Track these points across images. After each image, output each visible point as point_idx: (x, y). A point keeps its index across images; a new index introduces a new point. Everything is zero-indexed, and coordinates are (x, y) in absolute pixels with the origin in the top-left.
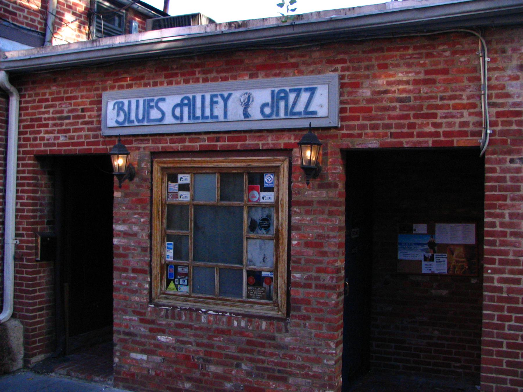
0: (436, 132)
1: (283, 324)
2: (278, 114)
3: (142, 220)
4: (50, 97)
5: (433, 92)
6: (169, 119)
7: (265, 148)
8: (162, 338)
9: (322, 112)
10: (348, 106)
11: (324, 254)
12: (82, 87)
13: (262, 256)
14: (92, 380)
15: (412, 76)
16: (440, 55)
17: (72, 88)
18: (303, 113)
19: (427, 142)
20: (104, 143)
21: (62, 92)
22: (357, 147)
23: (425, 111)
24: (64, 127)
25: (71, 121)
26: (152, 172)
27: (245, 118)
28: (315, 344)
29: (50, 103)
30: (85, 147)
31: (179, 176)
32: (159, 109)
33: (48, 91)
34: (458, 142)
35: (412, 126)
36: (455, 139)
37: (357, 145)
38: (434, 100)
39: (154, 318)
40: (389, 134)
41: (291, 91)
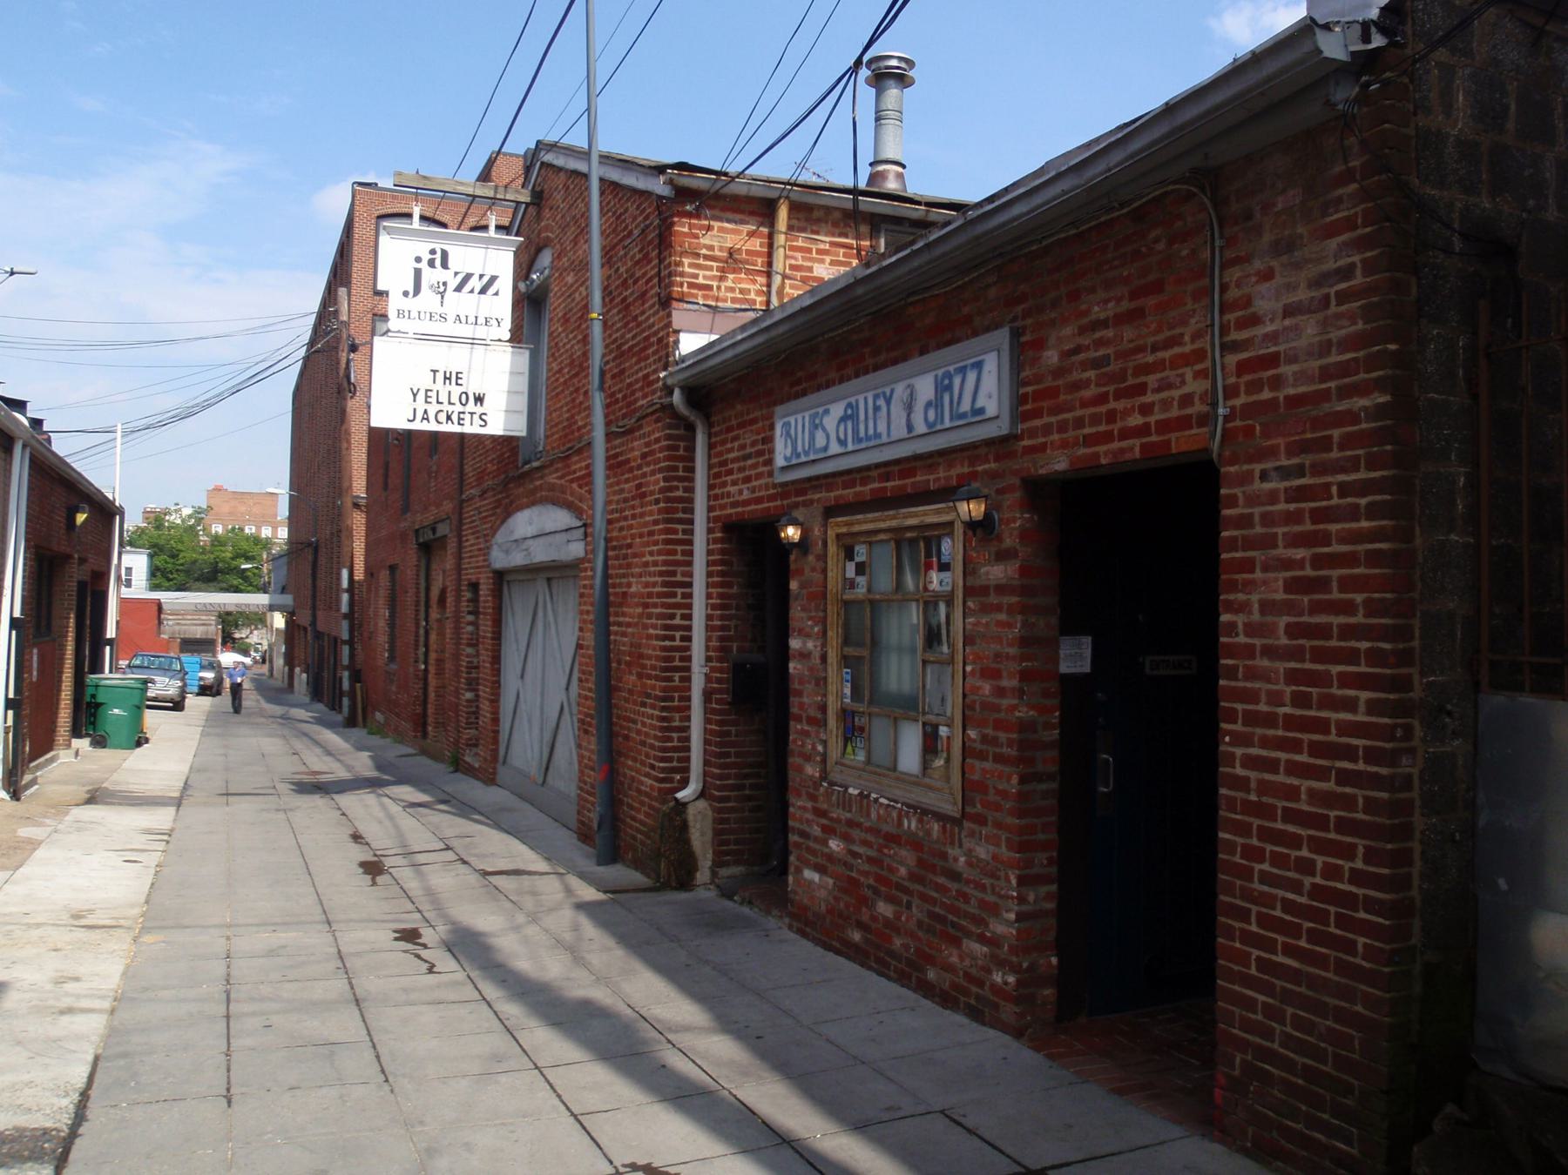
2: (942, 422)
19: (1131, 449)
32: (824, 430)
34: (1181, 442)
35: (1111, 417)
36: (1173, 436)
39: (825, 806)
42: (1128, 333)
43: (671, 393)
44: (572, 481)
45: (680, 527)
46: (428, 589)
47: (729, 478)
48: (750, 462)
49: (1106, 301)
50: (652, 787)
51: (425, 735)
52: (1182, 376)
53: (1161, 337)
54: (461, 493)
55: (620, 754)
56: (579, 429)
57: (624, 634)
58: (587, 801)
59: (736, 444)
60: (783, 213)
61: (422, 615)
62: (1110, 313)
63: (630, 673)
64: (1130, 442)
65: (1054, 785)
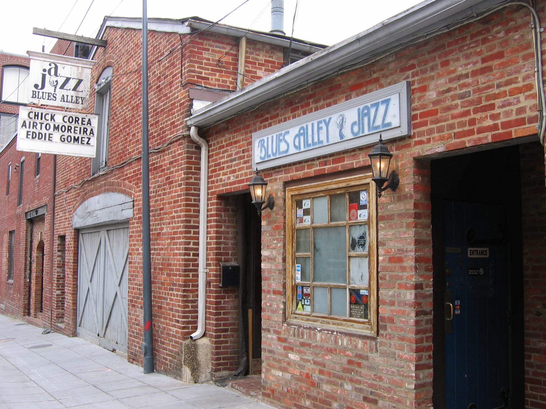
0: (494, 124)
1: (374, 343)
2: (363, 132)
3: (279, 245)
6: (292, 150)
10: (418, 112)
13: (360, 275)
14: (249, 395)
15: (470, 68)
16: (494, 38)
19: (486, 138)
22: (426, 153)
23: (484, 103)
28: (398, 366)
32: (286, 142)
33: (223, 139)
34: (517, 132)
35: (472, 122)
36: (513, 130)
37: (427, 151)
38: (491, 90)
39: (286, 336)
42: (482, 79)
43: (189, 129)
44: (124, 180)
45: (193, 198)
46: (31, 242)
47: (221, 172)
48: (234, 163)
49: (466, 65)
50: (177, 332)
51: (29, 314)
52: (518, 98)
53: (503, 80)
54: (55, 192)
55: (156, 316)
56: (130, 153)
57: (159, 254)
58: (134, 341)
59: (226, 154)
60: (243, 43)
61: (29, 255)
62: (470, 71)
63: (163, 274)
64: (485, 134)
65: (431, 317)
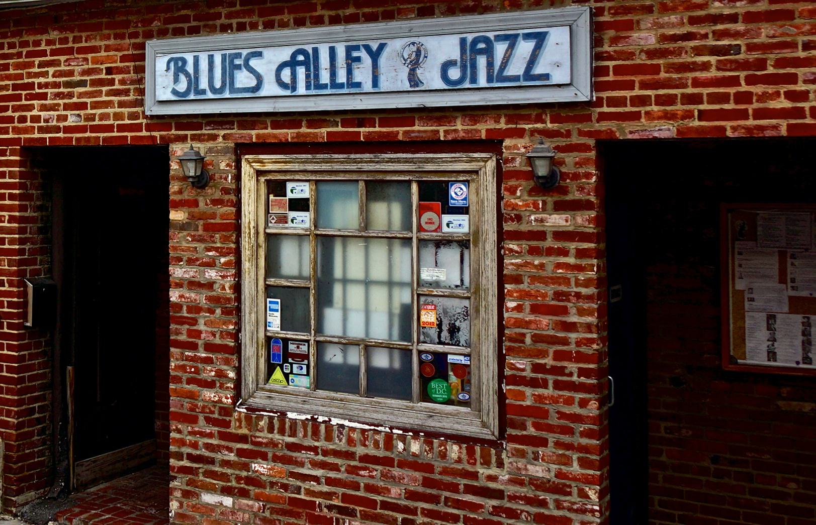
2: (474, 80)
3: (223, 260)
4: (48, 48)
5: (788, 35)
6: (270, 88)
7: (450, 137)
8: (260, 467)
9: (560, 76)
10: (611, 64)
11: (571, 327)
12: (106, 32)
17: (89, 33)
18: (522, 79)
19: (775, 127)
20: (149, 128)
21: (71, 39)
23: (771, 70)
24: (75, 100)
25: (88, 89)
26: (238, 178)
27: (411, 86)
29: (49, 58)
30: (115, 134)
31: (289, 185)
32: (252, 71)
33: (44, 37)
35: (745, 98)
37: (631, 133)
40: (696, 113)
41: (498, 38)
